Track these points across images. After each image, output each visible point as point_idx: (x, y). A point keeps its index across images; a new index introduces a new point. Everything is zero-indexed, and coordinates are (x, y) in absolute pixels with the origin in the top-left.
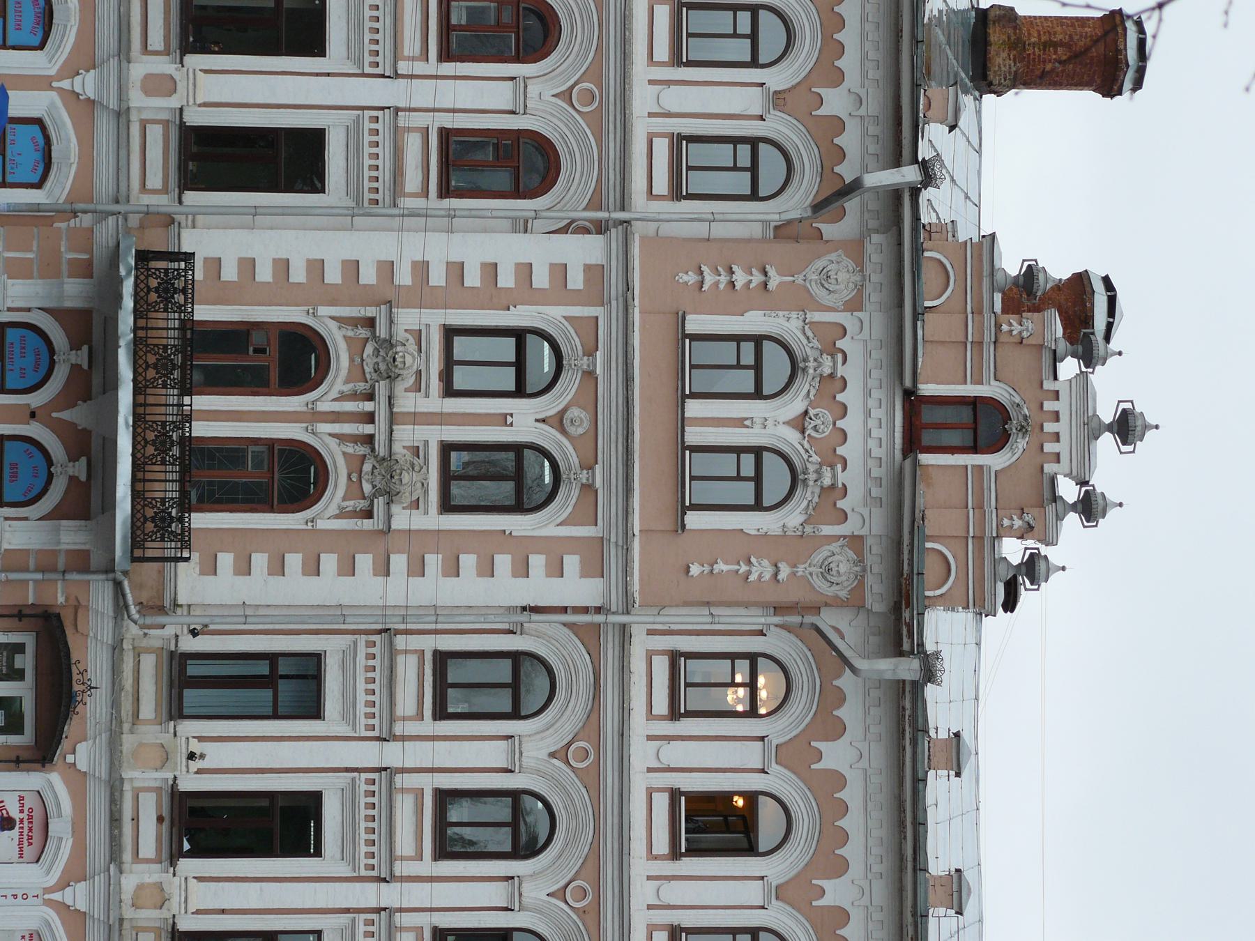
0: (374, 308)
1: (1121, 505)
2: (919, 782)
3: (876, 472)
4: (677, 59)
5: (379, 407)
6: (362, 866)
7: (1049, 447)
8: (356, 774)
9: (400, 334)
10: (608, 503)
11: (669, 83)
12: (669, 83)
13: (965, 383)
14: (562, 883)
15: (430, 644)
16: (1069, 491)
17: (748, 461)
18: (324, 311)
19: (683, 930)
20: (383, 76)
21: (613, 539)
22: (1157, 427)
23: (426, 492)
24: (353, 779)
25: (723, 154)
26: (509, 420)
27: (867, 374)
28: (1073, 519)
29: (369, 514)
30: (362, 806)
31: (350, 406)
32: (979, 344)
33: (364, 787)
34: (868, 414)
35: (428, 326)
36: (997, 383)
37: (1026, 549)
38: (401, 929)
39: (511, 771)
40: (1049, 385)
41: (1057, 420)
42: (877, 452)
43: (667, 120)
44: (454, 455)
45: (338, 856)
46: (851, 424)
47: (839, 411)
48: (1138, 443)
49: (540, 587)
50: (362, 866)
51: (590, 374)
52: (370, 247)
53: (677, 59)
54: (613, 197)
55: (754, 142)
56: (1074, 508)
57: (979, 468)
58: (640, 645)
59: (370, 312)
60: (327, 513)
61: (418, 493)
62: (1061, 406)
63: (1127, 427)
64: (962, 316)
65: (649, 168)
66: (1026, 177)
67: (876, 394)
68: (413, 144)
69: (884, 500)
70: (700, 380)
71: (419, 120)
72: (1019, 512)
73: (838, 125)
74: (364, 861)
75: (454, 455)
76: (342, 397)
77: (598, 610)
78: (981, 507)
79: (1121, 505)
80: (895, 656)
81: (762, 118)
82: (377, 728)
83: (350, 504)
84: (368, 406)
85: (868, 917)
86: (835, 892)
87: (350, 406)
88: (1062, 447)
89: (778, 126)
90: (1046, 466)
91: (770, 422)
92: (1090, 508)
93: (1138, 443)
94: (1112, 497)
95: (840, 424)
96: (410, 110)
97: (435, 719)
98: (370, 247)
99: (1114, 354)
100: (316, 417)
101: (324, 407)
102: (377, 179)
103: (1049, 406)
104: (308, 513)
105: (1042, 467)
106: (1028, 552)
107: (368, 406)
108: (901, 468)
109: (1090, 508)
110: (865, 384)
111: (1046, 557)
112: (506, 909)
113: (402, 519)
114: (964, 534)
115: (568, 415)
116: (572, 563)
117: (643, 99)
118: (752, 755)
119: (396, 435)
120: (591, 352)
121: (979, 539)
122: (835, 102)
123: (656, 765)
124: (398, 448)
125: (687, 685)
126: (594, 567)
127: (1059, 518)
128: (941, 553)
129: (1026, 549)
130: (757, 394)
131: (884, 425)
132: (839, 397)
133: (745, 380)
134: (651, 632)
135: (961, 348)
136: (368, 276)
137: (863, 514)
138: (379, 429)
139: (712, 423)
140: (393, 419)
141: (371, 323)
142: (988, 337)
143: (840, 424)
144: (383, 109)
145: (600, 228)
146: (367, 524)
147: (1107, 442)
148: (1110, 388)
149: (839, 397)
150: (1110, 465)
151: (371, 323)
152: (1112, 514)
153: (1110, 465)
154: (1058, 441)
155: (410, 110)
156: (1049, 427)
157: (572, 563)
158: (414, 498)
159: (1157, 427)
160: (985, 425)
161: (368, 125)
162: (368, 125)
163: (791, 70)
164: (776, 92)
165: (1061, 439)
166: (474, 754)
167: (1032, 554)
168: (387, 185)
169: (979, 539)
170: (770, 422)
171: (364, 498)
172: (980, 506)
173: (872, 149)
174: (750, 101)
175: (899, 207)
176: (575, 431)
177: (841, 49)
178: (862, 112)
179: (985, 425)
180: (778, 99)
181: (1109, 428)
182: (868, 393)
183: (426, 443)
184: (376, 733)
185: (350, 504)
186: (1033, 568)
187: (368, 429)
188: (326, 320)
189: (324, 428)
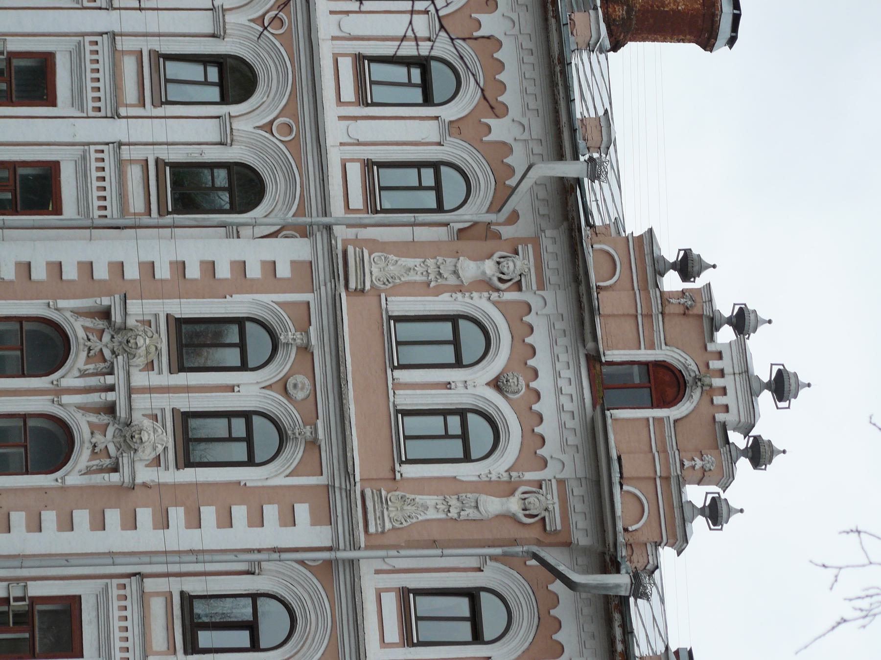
0: (108, 298)
1: (770, 322)
2: (564, 63)
3: (570, 424)
4: (363, 100)
5: (117, 379)
6: (90, 108)
7: (719, 400)
8: (86, 147)
9: (131, 322)
10: (329, 455)
11: (355, 118)
12: (355, 118)
13: (640, 348)
14: (260, 13)
15: (176, 586)
16: (737, 439)
17: (454, 422)
18: (62, 304)
19: (410, 591)
20: (100, 8)
21: (337, 484)
22: (809, 385)
23: (159, 355)
24: (84, 151)
25: (410, 177)
26: (236, 389)
27: (554, 343)
28: (743, 464)
29: (115, 469)
30: (116, 618)
31: (93, 381)
32: (649, 316)
33: (94, 155)
34: (557, 375)
35: (163, 410)
36: (668, 348)
37: (707, 493)
38: (123, 52)
39: (253, 574)
40: (711, 347)
41: (725, 394)
42: (568, 406)
43: (350, 43)
44: (183, 326)
45: (69, 102)
46: (543, 384)
47: (531, 374)
48: (793, 400)
49: (274, 534)
50: (90, 108)
51: (305, 349)
52: (104, 251)
53: (363, 100)
54: (315, 205)
55: (436, 166)
56: (744, 453)
57: (659, 421)
58: (369, 583)
59: (106, 301)
60: (74, 474)
61: (153, 356)
62: (727, 382)
63: (782, 386)
64: (650, 456)
65: (346, 189)
66: (670, 140)
67: (562, 341)
68: (129, 66)
69: (580, 448)
70: (415, 449)
71: (138, 153)
72: (698, 453)
73: (506, 148)
74: (91, 104)
75: (183, 326)
76: (89, 471)
77: (330, 549)
78: (665, 451)
79: (770, 322)
80: (602, 573)
81: (439, 144)
82: (103, 109)
83: (91, 367)
84: (110, 380)
85: (551, 326)
86: (501, 130)
87: (93, 381)
88: (728, 400)
89: (454, 150)
90: (711, 363)
91: (471, 386)
92: (760, 454)
93: (793, 400)
94: (763, 315)
95: (533, 385)
96: (129, 144)
97: (186, 653)
98: (104, 251)
99: (764, 322)
100: (59, 391)
101: (67, 382)
102: (103, 179)
103: (715, 364)
104: (55, 376)
105: (714, 417)
106: (710, 497)
107: (110, 380)
108: (593, 419)
109: (760, 454)
110: (554, 368)
111: (726, 500)
112: (221, 144)
113: (145, 474)
114: (633, 312)
115: (291, 381)
116: (302, 511)
117: (335, 132)
118: (429, 131)
119: (135, 405)
120: (304, 327)
121: (666, 479)
122: (501, 130)
123: (338, 33)
124: (137, 417)
125: (381, 188)
126: (324, 515)
127: (733, 462)
128: (608, 253)
129: (707, 493)
130: (458, 363)
131: (588, 516)
132: (535, 407)
133: (455, 448)
134: (377, 572)
135: (652, 482)
136: (101, 273)
137: (563, 461)
138: (118, 397)
139: (417, 389)
140: (130, 391)
141: (106, 314)
142: (656, 309)
143: (533, 385)
144: (107, 144)
145: (304, 232)
146: (115, 477)
147: (766, 398)
148: (764, 354)
149: (528, 340)
150: (771, 420)
151: (106, 314)
152: (777, 460)
153: (771, 420)
154: (727, 411)
155: (129, 144)
156: (717, 382)
157: (302, 511)
158: (149, 360)
159: (809, 385)
160: (664, 384)
161: (88, 48)
162: (88, 48)
163: (461, 105)
164: (451, 122)
165: (724, 355)
166: (192, 131)
167: (713, 499)
168: (136, 632)
169: (666, 479)
170: (471, 386)
171: (110, 457)
172: (663, 451)
173: (530, 90)
174: (429, 131)
175: (568, 193)
176: (300, 395)
177: (538, 395)
178: (526, 136)
179: (664, 384)
180: (454, 127)
181: (768, 386)
182: (555, 358)
183: (163, 410)
184: (102, 114)
185: (91, 367)
186: (716, 513)
187: (110, 396)
188: (66, 311)
189: (66, 399)
